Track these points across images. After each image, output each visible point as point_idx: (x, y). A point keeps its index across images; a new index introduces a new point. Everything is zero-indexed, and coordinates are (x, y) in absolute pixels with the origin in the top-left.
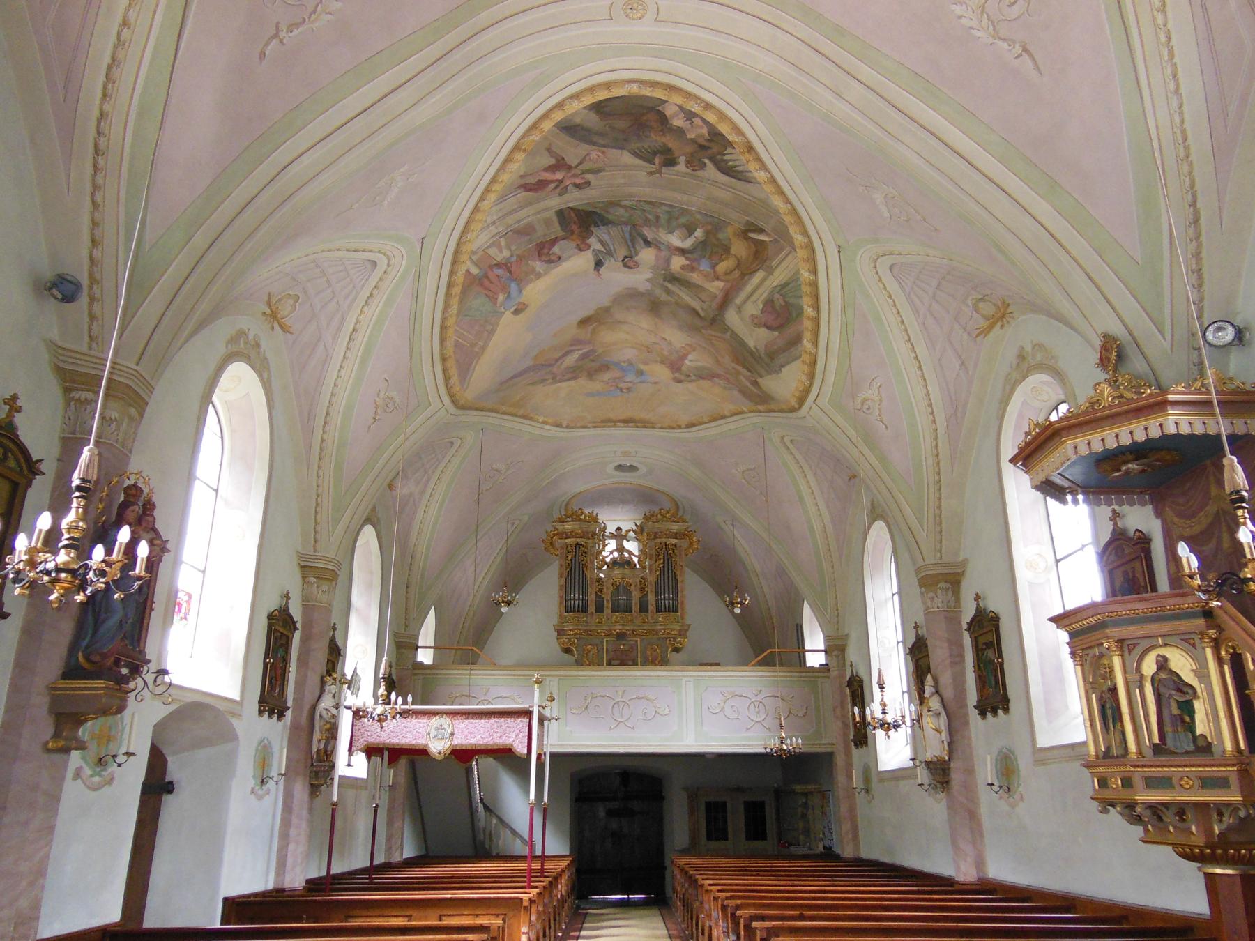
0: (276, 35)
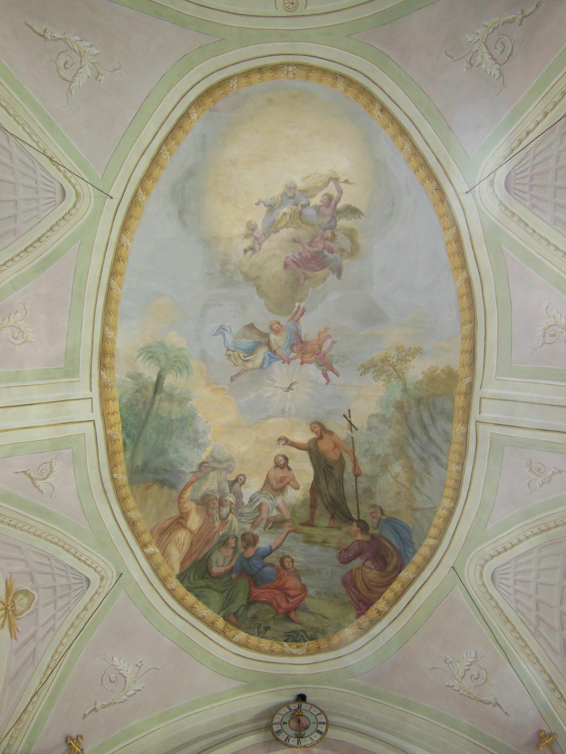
0: (524, 17)
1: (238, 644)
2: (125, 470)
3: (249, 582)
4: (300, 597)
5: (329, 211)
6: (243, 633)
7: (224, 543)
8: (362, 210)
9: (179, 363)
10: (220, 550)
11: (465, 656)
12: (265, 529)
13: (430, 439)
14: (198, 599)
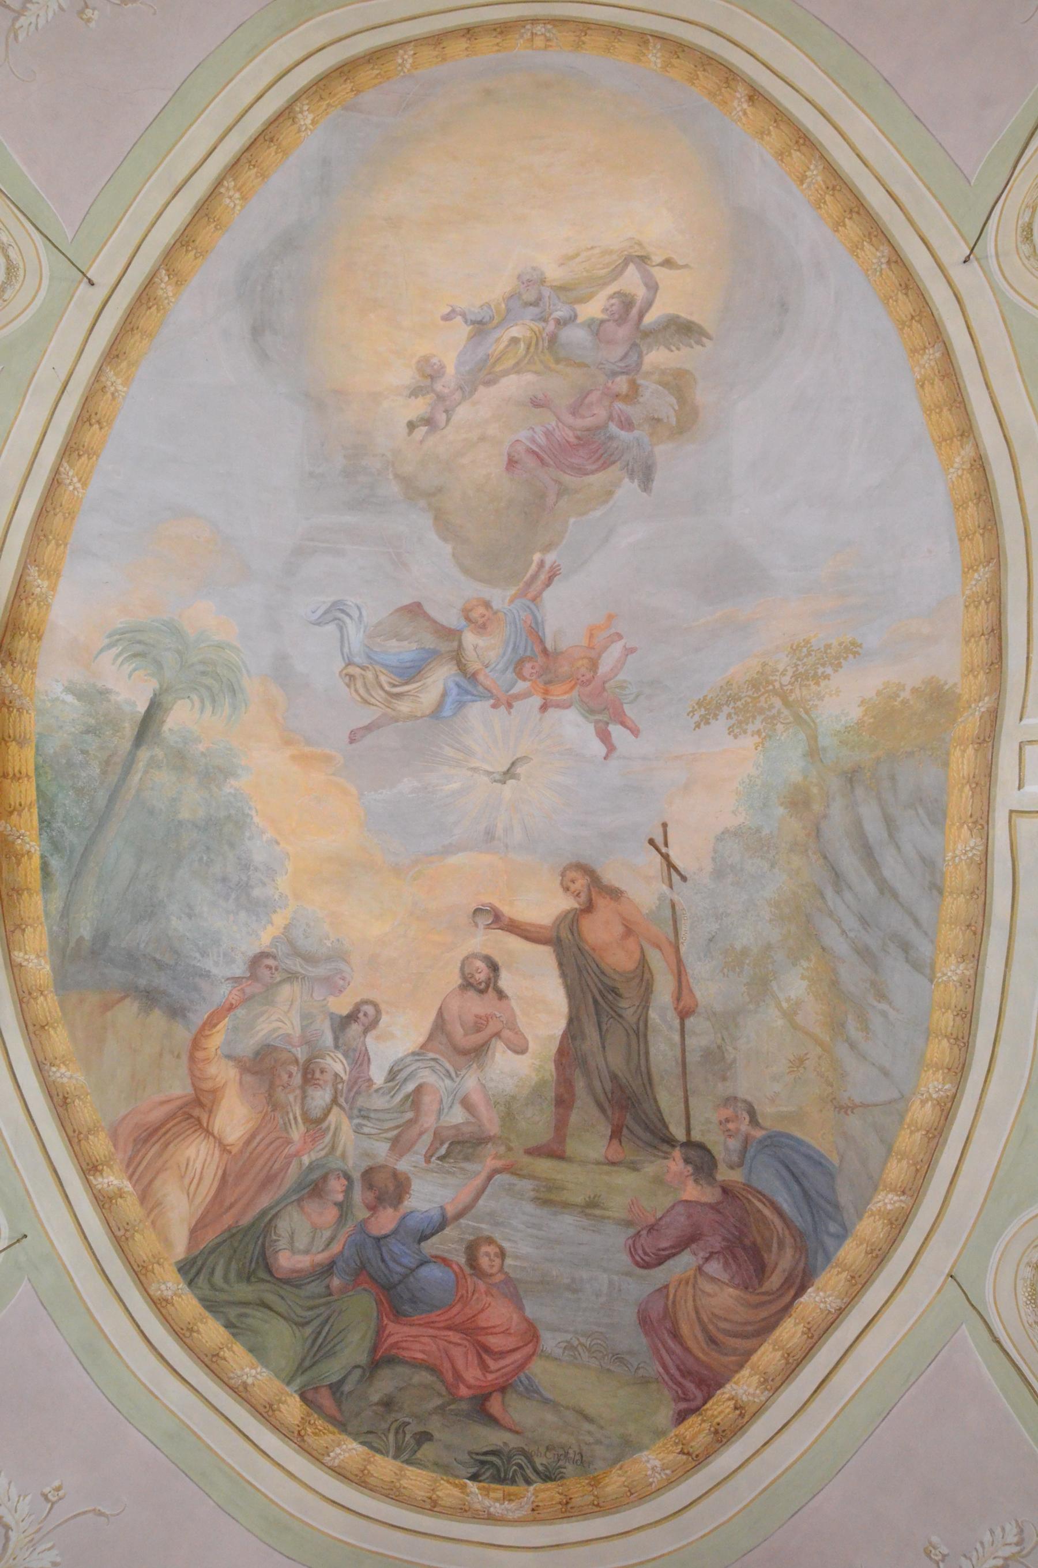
1: (339, 1473)
2: (46, 944)
3: (379, 1303)
4: (518, 1356)
5: (623, 332)
6: (355, 1445)
7: (313, 1187)
8: (707, 326)
9: (213, 679)
10: (302, 1208)
11: (987, 1538)
12: (428, 1160)
13: (884, 887)
14: (234, 1335)
